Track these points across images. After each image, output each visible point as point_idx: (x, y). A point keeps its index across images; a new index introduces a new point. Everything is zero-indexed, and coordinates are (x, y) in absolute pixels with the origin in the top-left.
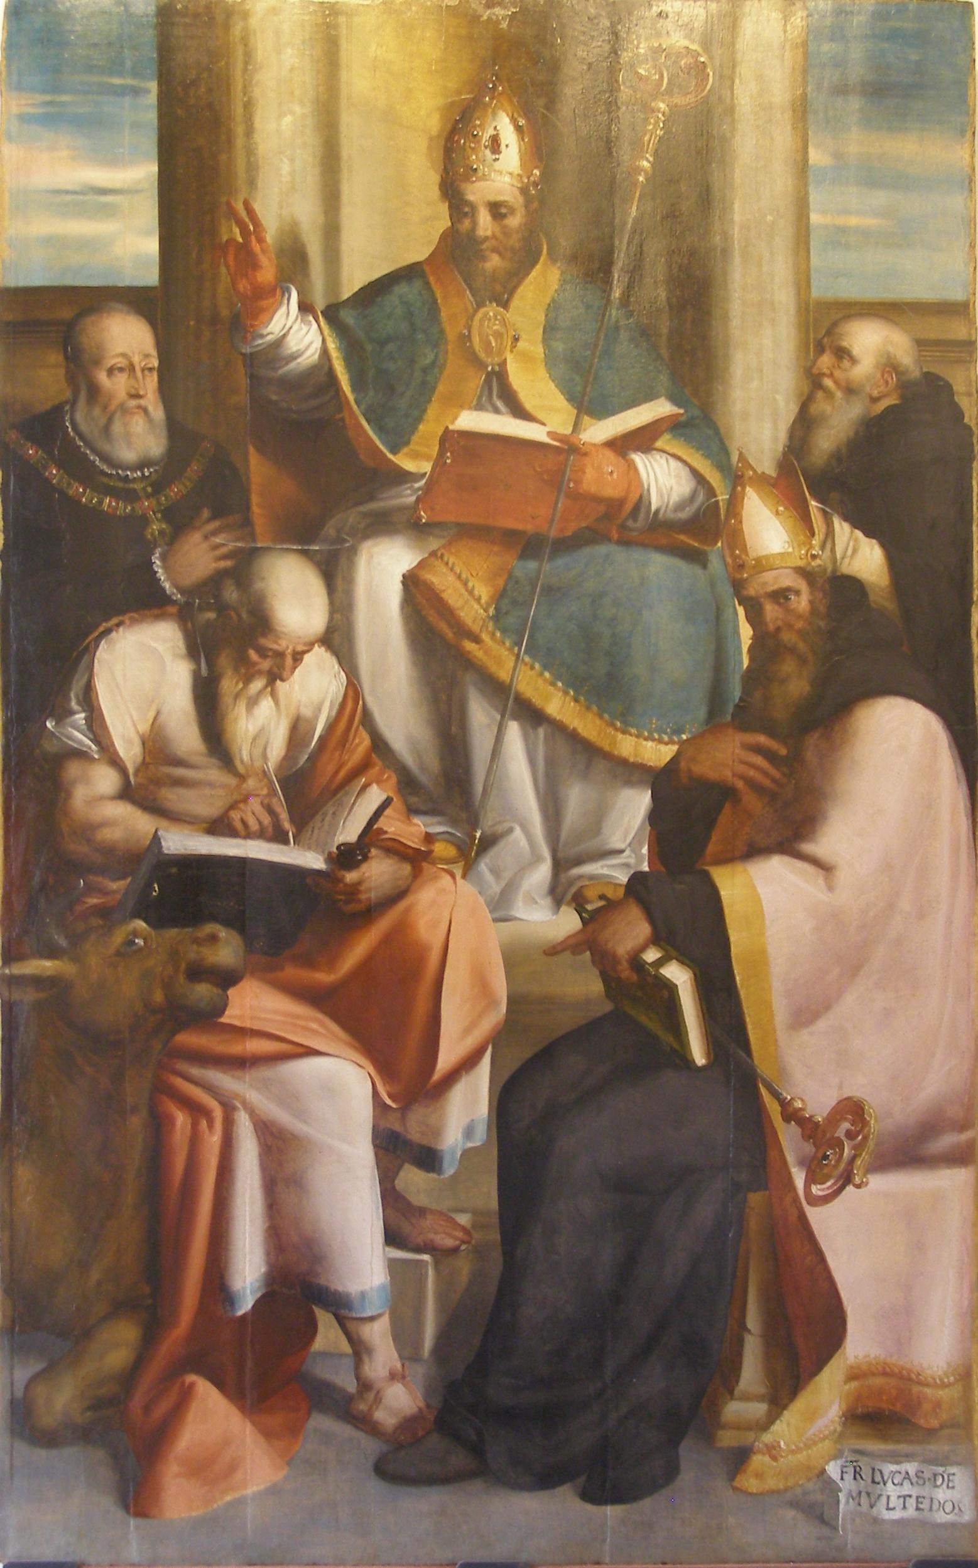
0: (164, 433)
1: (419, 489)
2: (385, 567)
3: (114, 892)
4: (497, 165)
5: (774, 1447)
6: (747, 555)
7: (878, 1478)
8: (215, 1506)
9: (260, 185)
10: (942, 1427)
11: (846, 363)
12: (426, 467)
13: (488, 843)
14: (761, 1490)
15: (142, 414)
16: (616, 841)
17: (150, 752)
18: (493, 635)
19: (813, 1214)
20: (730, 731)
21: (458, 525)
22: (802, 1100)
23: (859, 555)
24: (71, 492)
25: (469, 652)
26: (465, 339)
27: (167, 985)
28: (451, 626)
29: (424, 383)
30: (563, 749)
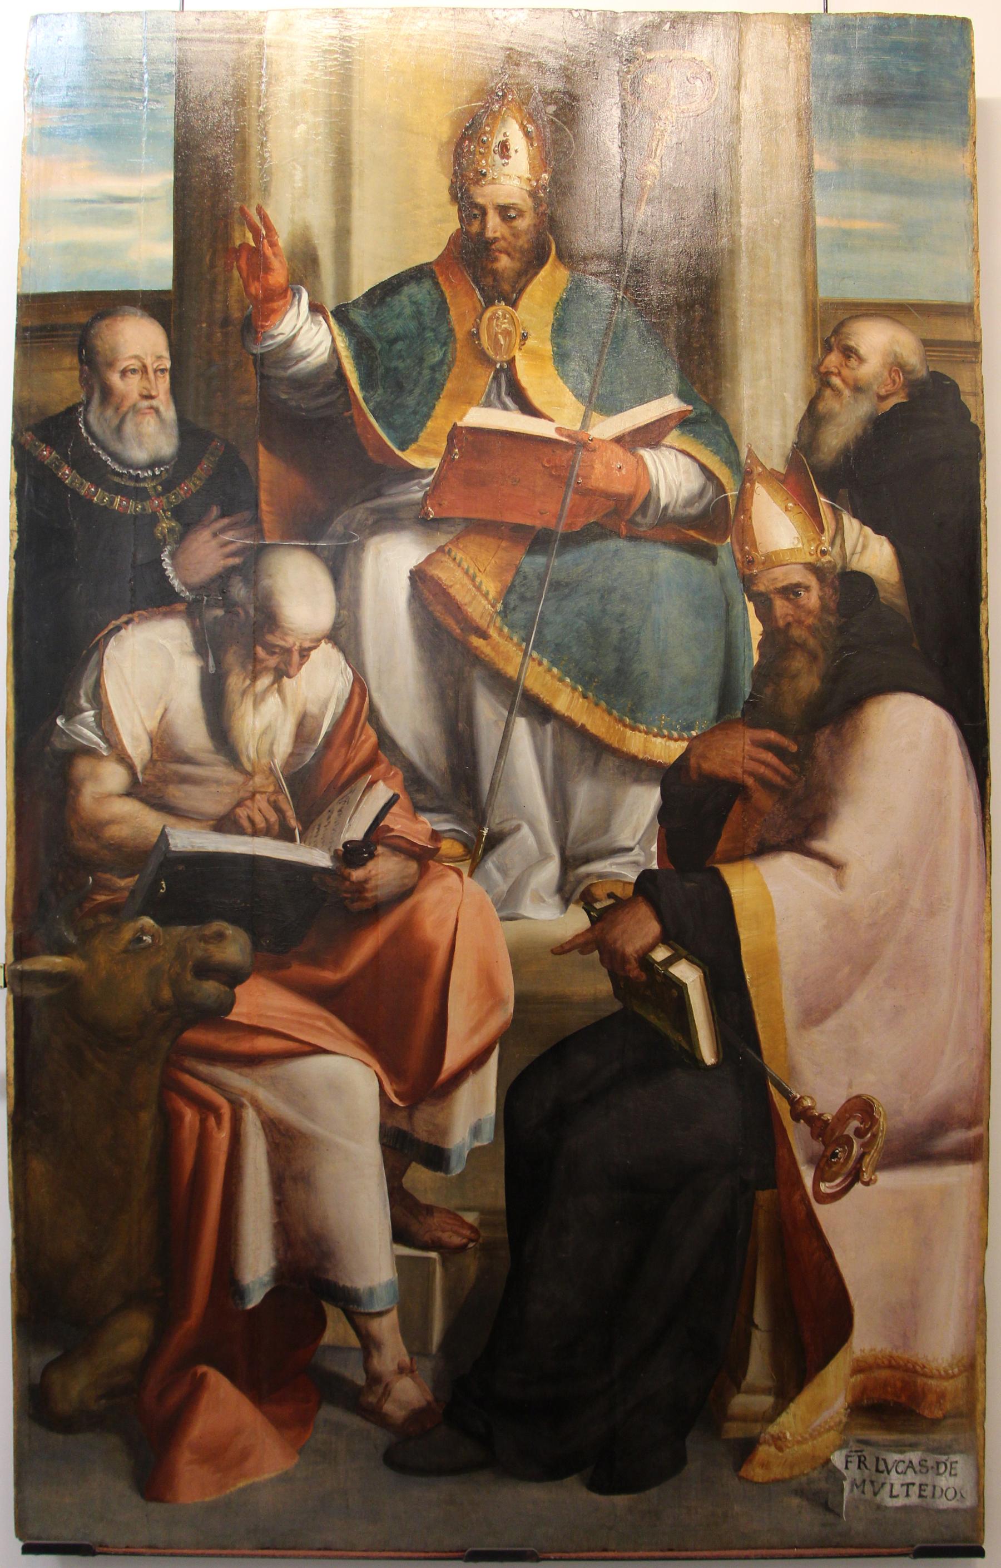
0: (175, 432)
1: (428, 485)
2: (392, 561)
3: (121, 889)
4: (506, 170)
5: (779, 1438)
6: (757, 550)
7: (882, 1467)
8: (228, 1492)
9: (273, 190)
10: (945, 1417)
11: (853, 362)
12: (434, 463)
13: (495, 841)
14: (766, 1479)
15: (154, 415)
16: (625, 838)
17: (157, 748)
18: (500, 631)
19: (823, 1213)
20: (740, 727)
21: (465, 519)
22: (812, 1098)
23: (868, 552)
24: (83, 492)
25: (476, 648)
26: (474, 336)
27: (175, 983)
28: (458, 622)
29: (433, 380)
30: (572, 746)
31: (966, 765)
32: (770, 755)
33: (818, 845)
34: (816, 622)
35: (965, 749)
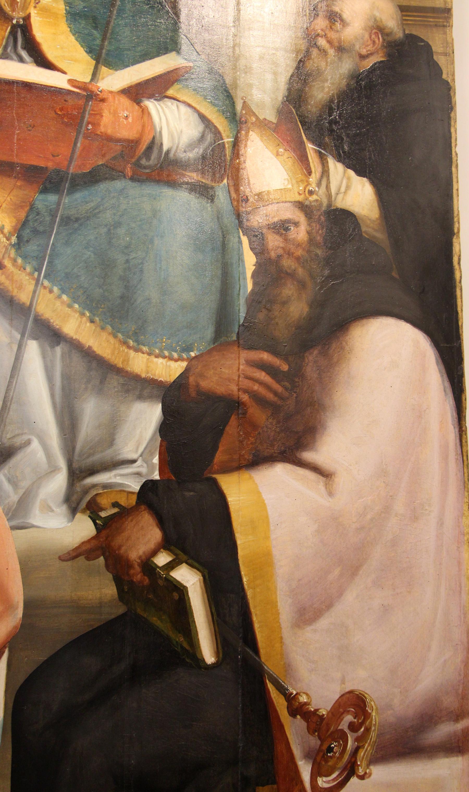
16: (128, 452)
18: (15, 261)
20: (236, 348)
22: (307, 694)
23: (351, 193)
31: (443, 381)
32: (264, 374)
33: (308, 456)
34: (304, 253)
35: (442, 367)
